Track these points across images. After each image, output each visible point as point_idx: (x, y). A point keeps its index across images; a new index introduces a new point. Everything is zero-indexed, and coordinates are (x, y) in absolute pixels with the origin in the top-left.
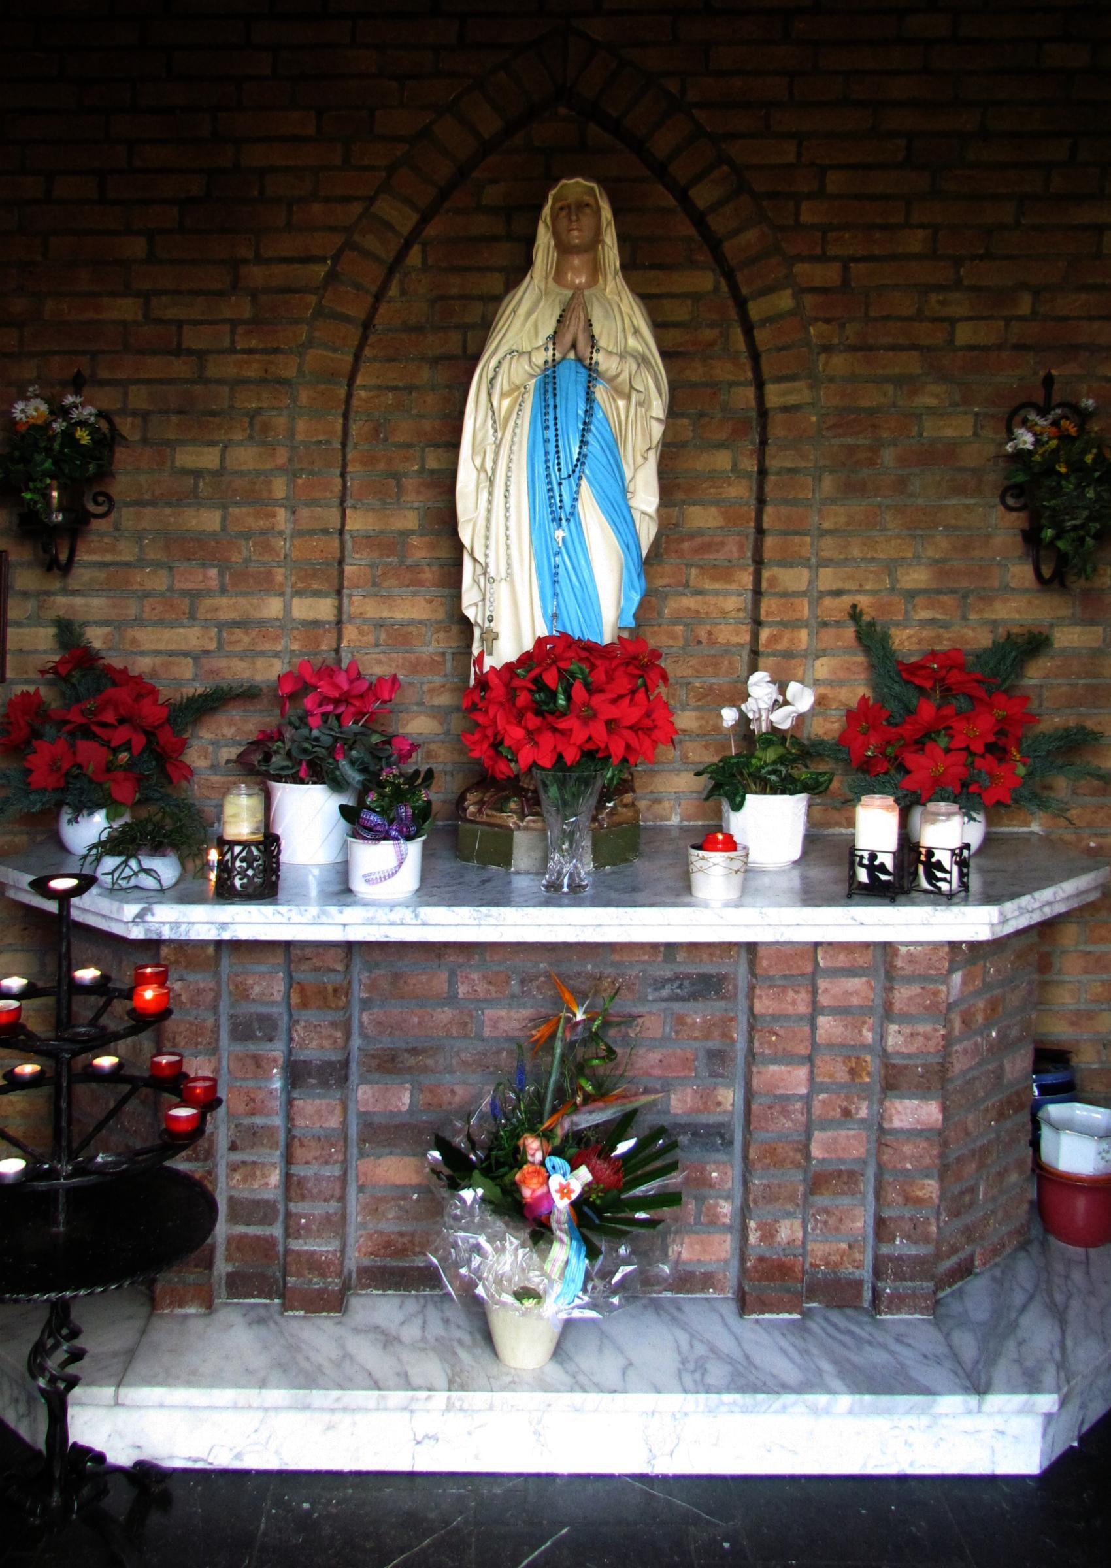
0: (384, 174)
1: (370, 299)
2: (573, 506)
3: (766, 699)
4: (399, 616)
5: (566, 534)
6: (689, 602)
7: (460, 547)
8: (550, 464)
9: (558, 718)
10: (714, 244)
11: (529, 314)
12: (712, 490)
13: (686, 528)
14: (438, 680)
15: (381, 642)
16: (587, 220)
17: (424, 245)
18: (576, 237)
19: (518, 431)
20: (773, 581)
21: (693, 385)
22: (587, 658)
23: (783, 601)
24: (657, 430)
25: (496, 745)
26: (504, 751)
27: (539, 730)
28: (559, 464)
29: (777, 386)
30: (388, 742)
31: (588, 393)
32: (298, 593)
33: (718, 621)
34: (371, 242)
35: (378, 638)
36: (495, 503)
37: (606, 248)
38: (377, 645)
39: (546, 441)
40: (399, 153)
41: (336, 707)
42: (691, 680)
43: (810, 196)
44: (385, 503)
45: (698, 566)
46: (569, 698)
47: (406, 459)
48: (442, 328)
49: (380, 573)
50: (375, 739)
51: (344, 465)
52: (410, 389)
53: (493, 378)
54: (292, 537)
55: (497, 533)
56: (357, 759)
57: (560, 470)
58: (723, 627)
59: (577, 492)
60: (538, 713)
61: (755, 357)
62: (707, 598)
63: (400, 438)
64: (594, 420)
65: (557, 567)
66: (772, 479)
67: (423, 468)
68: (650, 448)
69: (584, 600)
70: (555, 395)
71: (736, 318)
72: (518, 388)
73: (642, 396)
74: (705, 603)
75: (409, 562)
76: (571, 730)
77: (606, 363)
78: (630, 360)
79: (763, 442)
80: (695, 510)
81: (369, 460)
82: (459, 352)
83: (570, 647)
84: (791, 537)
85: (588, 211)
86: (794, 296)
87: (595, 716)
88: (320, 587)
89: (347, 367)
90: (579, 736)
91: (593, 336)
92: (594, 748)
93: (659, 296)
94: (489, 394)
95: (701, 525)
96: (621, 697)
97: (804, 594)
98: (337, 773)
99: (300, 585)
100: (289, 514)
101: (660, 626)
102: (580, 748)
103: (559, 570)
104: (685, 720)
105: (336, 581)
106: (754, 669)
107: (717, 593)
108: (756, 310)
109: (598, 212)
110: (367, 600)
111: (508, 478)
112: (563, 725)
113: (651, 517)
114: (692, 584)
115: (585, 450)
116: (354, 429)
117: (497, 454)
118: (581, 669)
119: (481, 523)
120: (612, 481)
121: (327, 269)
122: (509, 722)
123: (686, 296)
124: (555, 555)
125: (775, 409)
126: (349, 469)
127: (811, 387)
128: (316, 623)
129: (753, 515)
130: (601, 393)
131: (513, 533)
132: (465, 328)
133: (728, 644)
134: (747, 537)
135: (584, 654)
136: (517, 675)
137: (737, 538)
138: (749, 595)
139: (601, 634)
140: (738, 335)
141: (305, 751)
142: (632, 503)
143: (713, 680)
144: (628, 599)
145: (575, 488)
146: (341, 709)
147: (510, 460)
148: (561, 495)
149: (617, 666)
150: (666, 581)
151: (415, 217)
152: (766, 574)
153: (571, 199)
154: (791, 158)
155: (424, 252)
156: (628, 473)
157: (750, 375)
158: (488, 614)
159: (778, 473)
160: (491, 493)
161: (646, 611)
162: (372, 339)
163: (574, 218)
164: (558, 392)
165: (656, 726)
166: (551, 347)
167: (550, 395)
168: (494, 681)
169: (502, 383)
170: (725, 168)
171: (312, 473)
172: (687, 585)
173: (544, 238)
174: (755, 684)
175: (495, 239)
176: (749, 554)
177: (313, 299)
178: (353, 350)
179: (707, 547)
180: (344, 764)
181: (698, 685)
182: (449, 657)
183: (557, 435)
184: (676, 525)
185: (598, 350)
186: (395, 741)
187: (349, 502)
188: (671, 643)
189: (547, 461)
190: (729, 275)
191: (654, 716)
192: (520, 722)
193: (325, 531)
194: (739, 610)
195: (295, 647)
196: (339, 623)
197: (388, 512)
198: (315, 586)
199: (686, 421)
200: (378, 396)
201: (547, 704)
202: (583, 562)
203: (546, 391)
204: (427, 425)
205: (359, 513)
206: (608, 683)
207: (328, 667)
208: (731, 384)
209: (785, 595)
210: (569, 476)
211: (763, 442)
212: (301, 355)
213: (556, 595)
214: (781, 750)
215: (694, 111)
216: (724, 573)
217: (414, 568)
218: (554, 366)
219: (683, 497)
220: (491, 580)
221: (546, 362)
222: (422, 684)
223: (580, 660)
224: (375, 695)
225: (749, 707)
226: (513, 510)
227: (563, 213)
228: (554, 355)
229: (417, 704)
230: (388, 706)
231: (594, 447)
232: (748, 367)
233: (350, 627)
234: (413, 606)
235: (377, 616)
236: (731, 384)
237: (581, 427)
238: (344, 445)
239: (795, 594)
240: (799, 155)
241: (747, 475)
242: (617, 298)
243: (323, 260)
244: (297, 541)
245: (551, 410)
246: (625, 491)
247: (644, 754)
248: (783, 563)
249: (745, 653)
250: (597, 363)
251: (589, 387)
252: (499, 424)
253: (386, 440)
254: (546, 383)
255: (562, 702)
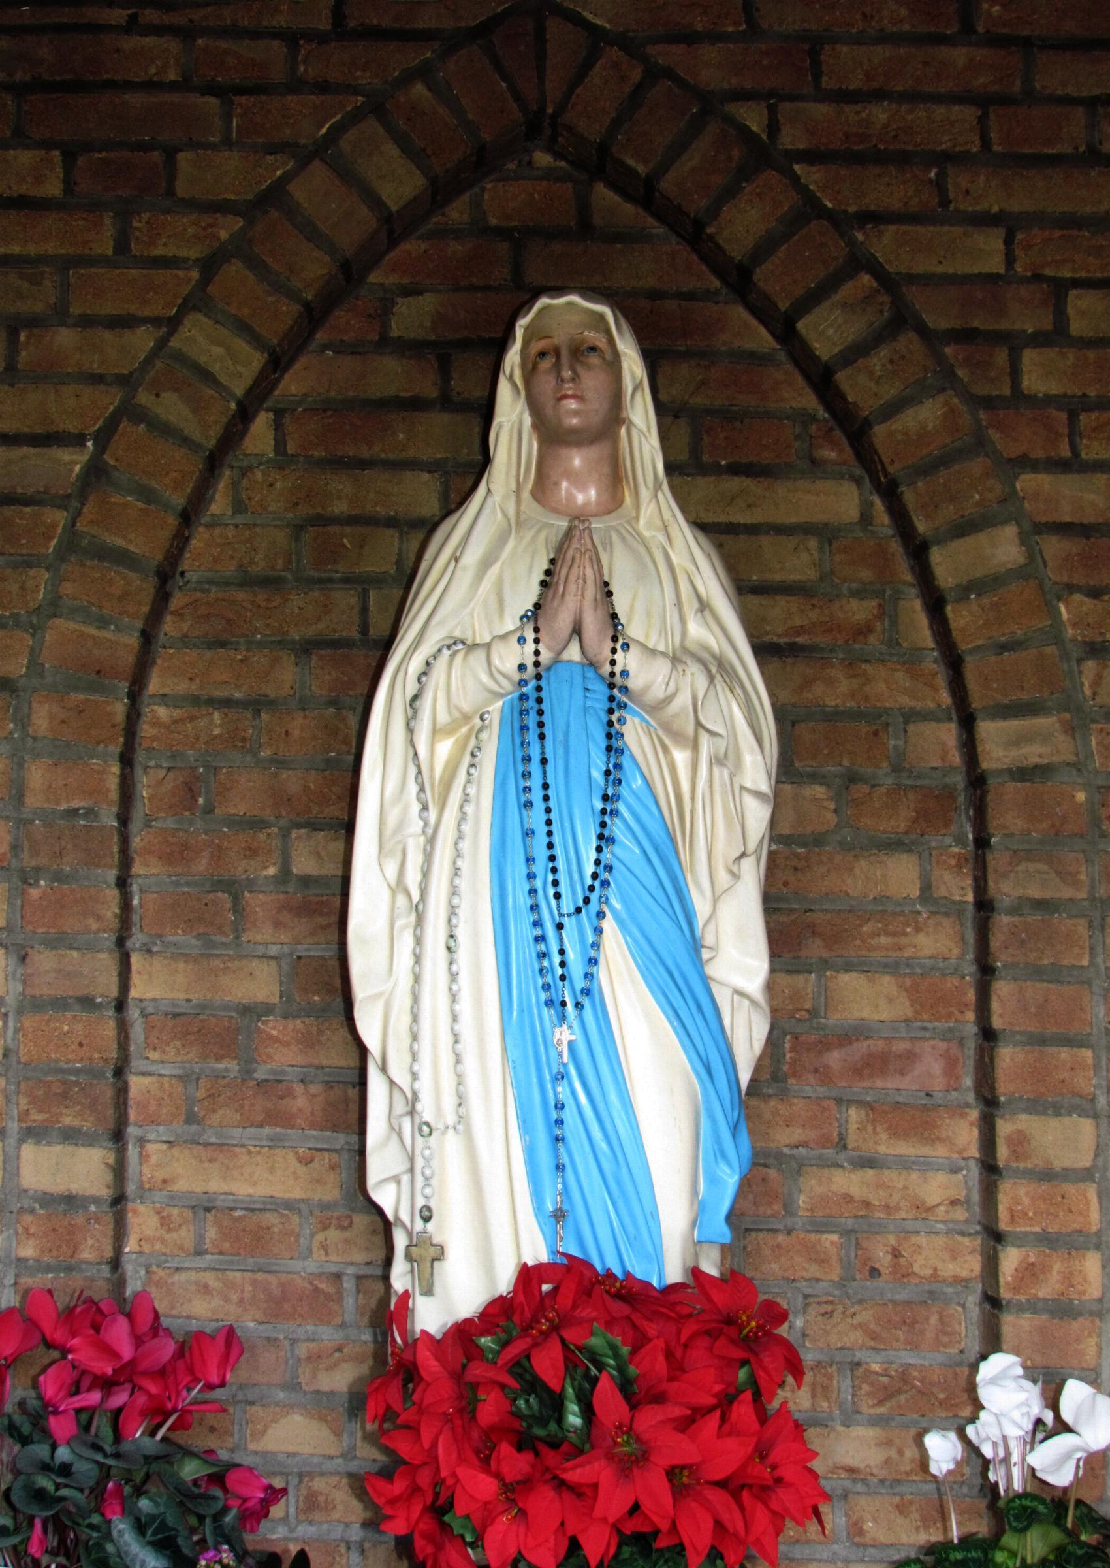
0: (195, 274)
1: (172, 521)
2: (588, 976)
3: (1016, 1415)
4: (243, 1189)
5: (577, 1036)
6: (849, 1182)
7: (363, 1051)
8: (538, 883)
9: (569, 1456)
10: (855, 431)
11: (486, 563)
12: (884, 940)
13: (833, 1020)
14: (328, 1335)
15: (207, 1245)
16: (593, 381)
17: (279, 413)
18: (572, 413)
19: (469, 809)
20: (1020, 1142)
21: (834, 716)
22: (628, 1318)
23: (1044, 1187)
24: (758, 816)
25: (440, 1509)
26: (453, 1520)
27: (527, 1484)
28: (555, 883)
29: (1001, 724)
30: (218, 1479)
31: (609, 736)
32: (34, 1134)
33: (909, 1225)
34: (171, 407)
35: (200, 1238)
36: (427, 963)
37: (634, 432)
38: (199, 1253)
39: (529, 833)
40: (224, 235)
41: (106, 1396)
42: (860, 1355)
43: (1040, 340)
44: (210, 944)
45: (860, 1103)
46: (588, 1412)
47: (252, 852)
48: (320, 581)
49: (201, 1093)
50: (190, 1470)
51: (126, 862)
52: (257, 705)
53: (415, 698)
54: (20, 1012)
55: (434, 1027)
56: (153, 1518)
57: (557, 896)
58: (922, 1239)
59: (596, 945)
60: (523, 1443)
61: (954, 662)
62: (888, 1175)
63: (239, 807)
64: (624, 790)
65: (560, 1107)
66: (1003, 921)
67: (285, 873)
68: (743, 855)
69: (619, 1182)
70: (542, 737)
71: (909, 578)
72: (466, 718)
73: (722, 744)
74: (881, 1186)
75: (260, 1074)
76: (595, 1486)
77: (643, 673)
78: (694, 668)
79: (982, 843)
80: (848, 981)
81: (177, 853)
82: (354, 633)
83: (589, 1294)
84: (1053, 1049)
85: (594, 360)
86: (1024, 539)
87: (643, 1457)
88: (76, 1122)
89: (127, 659)
90: (613, 1503)
91: (614, 616)
92: (646, 1529)
93: (753, 530)
94: (410, 730)
95: (865, 1014)
96: (697, 1414)
97: (1086, 1175)
98: (110, 1548)
99: (37, 1117)
100: (13, 961)
101: (789, 1232)
102: (616, 1528)
103: (564, 1118)
104: (847, 1448)
105: (110, 1112)
106: (992, 1343)
107: (905, 1164)
108: (947, 565)
109: (614, 364)
110: (175, 1151)
111: (453, 911)
112: (575, 1474)
113: (753, 1002)
114: (852, 1140)
115: (606, 856)
116: (144, 789)
117: (428, 857)
118: (613, 1347)
119: (402, 1001)
120: (667, 922)
121: (86, 457)
122: (461, 1460)
123: (807, 529)
124: (561, 1077)
125: (1001, 772)
126: (137, 868)
127: (1070, 730)
128: (70, 1201)
129: (971, 995)
130: (634, 733)
131: (466, 1027)
132: (363, 583)
133: (935, 1277)
134: (961, 1043)
135: (619, 1309)
136: (480, 1350)
137: (943, 1046)
138: (974, 1171)
139: (659, 1260)
140: (915, 611)
141: (40, 1496)
142: (710, 970)
143: (909, 1358)
144: (713, 1180)
145: (590, 938)
146: (120, 1398)
147: (456, 872)
148: (562, 952)
149: (692, 1337)
150: (797, 1134)
151: (257, 360)
152: (1004, 1128)
153: (560, 337)
154: (995, 264)
155: (278, 426)
156: (701, 907)
157: (946, 698)
158: (420, 1202)
159: (1015, 910)
160: (419, 941)
161: (754, 1211)
162: (177, 601)
163: (567, 374)
164: (547, 730)
165: (779, 1481)
166: (530, 635)
167: (532, 735)
168: (429, 1364)
169: (434, 708)
170: (866, 279)
171: (59, 877)
172: (842, 1145)
173: (510, 412)
174: (993, 1381)
175: (414, 404)
176: (968, 1082)
177: (60, 517)
178: (140, 624)
179: (877, 1064)
180: (122, 1527)
181: (875, 1367)
182: (348, 1285)
183: (549, 822)
184: (813, 1013)
185: (626, 646)
186: (231, 1479)
187: (137, 939)
188: (813, 1270)
189: (531, 876)
190: (890, 492)
191: (776, 1455)
192: (487, 1459)
193: (87, 1002)
194: (954, 1203)
195: (28, 1251)
196: (119, 1200)
197: (217, 962)
198: (68, 1121)
199: (819, 791)
200: (192, 719)
201: (543, 1422)
202: (613, 1097)
203: (524, 728)
204: (292, 781)
205: (158, 964)
206: (671, 1379)
207: (90, 1301)
208: (911, 716)
209: (1048, 1175)
210: (578, 910)
211: (982, 843)
212: (35, 630)
213: (560, 1168)
214: (1056, 1536)
215: (796, 167)
216: (917, 1119)
217: (272, 1086)
218: (538, 677)
219: (825, 954)
220: (425, 1130)
221: (522, 667)
222: (294, 1342)
223: (609, 1324)
224: (191, 1370)
225: (985, 1432)
226: (464, 980)
227: (546, 364)
228: (537, 653)
229: (285, 1387)
230: (219, 1394)
231: (626, 849)
232: (941, 681)
233: (142, 1208)
234: (272, 1170)
235: (198, 1188)
236: (911, 716)
237: (599, 805)
238: (124, 819)
239: (1067, 1175)
240: (1010, 260)
241: (954, 910)
242: (661, 537)
243: (78, 440)
244: (29, 1022)
245: (535, 767)
246: (695, 945)
247: (758, 1543)
248: (1038, 1106)
249: (973, 1300)
250: (625, 673)
251: (610, 724)
252: (433, 793)
253: (209, 810)
254: (523, 712)
255: (574, 1419)
